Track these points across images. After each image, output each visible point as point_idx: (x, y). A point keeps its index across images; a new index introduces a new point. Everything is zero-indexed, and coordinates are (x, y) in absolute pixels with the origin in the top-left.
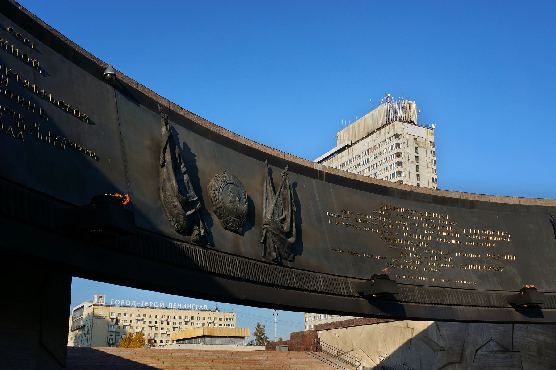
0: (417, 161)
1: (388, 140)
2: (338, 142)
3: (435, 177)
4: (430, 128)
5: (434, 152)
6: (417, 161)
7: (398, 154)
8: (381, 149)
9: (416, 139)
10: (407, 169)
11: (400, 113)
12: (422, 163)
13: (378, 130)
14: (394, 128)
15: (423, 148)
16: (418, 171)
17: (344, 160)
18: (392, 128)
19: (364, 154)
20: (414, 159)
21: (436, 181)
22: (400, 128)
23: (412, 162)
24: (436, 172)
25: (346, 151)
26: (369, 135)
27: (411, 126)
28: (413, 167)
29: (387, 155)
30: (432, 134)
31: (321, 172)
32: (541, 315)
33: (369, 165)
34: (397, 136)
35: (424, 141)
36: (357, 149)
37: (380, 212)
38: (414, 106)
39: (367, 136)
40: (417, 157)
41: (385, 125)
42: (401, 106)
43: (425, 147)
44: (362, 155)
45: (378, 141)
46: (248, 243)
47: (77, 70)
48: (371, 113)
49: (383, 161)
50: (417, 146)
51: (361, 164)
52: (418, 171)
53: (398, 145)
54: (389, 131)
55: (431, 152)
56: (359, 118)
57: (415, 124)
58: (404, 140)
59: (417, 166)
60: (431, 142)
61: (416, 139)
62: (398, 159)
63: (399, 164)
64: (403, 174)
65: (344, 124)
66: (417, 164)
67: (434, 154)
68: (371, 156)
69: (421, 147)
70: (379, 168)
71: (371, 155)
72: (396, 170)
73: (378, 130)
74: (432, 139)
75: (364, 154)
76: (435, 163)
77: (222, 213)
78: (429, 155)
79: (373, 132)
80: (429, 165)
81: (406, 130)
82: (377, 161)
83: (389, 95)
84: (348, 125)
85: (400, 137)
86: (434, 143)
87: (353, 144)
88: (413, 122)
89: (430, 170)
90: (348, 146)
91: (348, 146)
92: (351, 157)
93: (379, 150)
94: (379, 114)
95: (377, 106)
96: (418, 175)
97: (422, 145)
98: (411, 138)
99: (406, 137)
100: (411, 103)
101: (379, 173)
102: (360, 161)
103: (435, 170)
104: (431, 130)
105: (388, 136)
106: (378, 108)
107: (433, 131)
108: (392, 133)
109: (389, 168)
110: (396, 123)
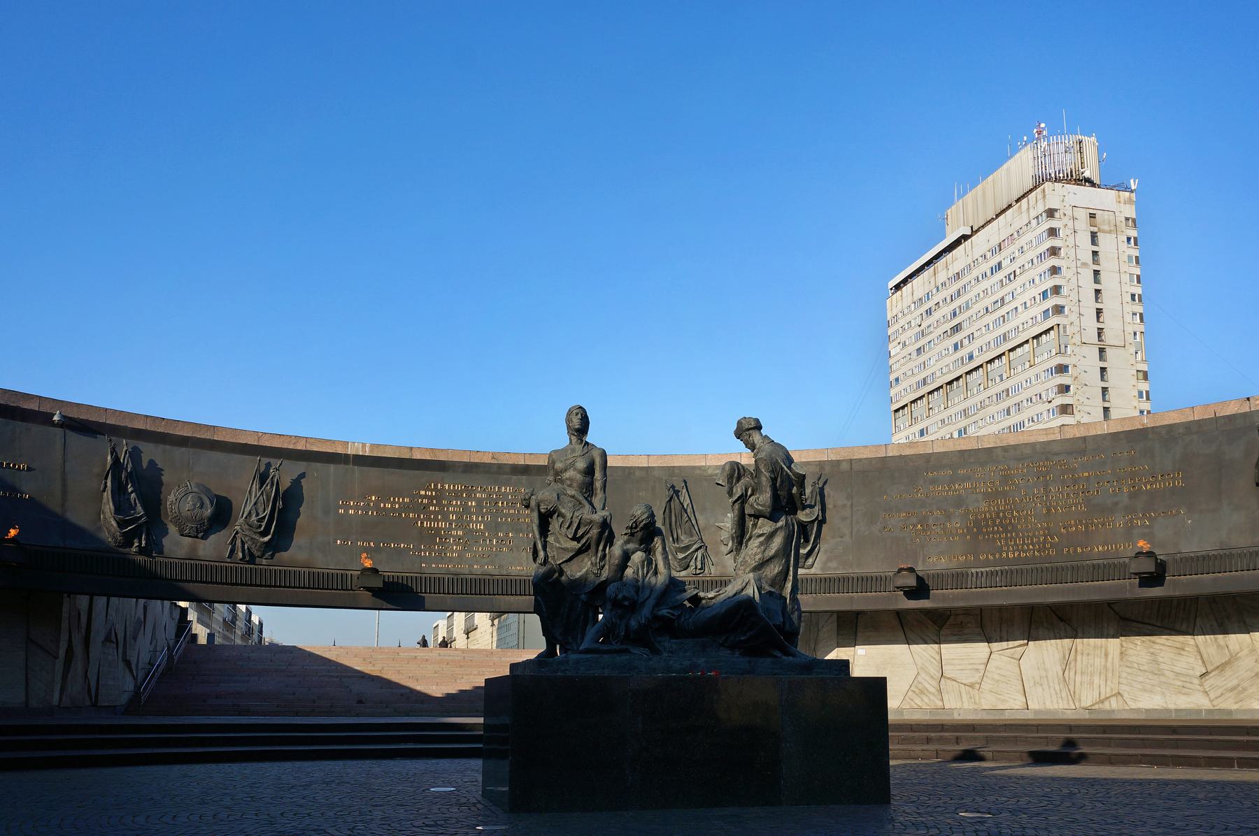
0: (1095, 262)
1: (1034, 222)
2: (948, 229)
3: (1138, 290)
4: (1127, 189)
5: (1135, 239)
6: (1095, 262)
7: (1054, 251)
8: (1023, 241)
9: (1092, 216)
10: (1074, 280)
11: (1067, 163)
12: (1106, 266)
13: (1018, 201)
14: (1044, 197)
15: (1110, 232)
16: (1097, 281)
17: (956, 267)
18: (1040, 196)
19: (993, 251)
20: (1088, 258)
21: (1140, 300)
22: (1056, 195)
23: (1085, 265)
24: (1139, 282)
25: (961, 248)
26: (1003, 211)
27: (1088, 189)
28: (1088, 275)
29: (1032, 254)
30: (1130, 201)
31: (347, 456)
32: (210, 617)
33: (1000, 275)
34: (1051, 213)
35: (1112, 218)
36: (980, 243)
37: (423, 493)
38: (1090, 143)
39: (998, 216)
40: (1095, 253)
41: (1031, 191)
42: (1062, 148)
43: (1116, 230)
44: (989, 254)
45: (1016, 226)
46: (212, 547)
47: (20, 426)
48: (1005, 166)
49: (1027, 267)
50: (1095, 229)
51: (989, 273)
52: (1097, 281)
53: (1053, 232)
54: (1036, 204)
55: (1129, 239)
56: (984, 178)
57: (1093, 184)
58: (1065, 220)
59: (1096, 273)
60: (1127, 219)
61: (1092, 216)
62: (1054, 261)
63: (1055, 270)
64: (1064, 291)
65: (959, 190)
66: (1097, 268)
67: (1136, 244)
68: (1003, 257)
69: (1104, 232)
70: (1020, 280)
71: (1004, 253)
72: (1050, 282)
73: (1018, 201)
74: (1131, 212)
75: (993, 251)
76: (1137, 262)
77: (178, 521)
78: (1123, 246)
79: (1010, 206)
80: (1124, 268)
81: (1071, 200)
82: (1015, 267)
83: (1043, 125)
84: (965, 193)
85: (1057, 215)
86: (1134, 221)
87: (974, 232)
88: (1089, 181)
89: (1126, 278)
90: (965, 237)
91: (965, 237)
92: (970, 261)
93: (1018, 244)
94: (1020, 167)
95: (1015, 150)
96: (1098, 292)
97: (1106, 228)
98: (1083, 216)
99: (1069, 212)
100: (1085, 139)
101: (1019, 290)
102: (985, 267)
103: (1138, 277)
104: (1127, 194)
105: (1033, 214)
106: (1017, 156)
107: (1133, 195)
108: (1041, 208)
109: (1037, 280)
110: (1047, 185)
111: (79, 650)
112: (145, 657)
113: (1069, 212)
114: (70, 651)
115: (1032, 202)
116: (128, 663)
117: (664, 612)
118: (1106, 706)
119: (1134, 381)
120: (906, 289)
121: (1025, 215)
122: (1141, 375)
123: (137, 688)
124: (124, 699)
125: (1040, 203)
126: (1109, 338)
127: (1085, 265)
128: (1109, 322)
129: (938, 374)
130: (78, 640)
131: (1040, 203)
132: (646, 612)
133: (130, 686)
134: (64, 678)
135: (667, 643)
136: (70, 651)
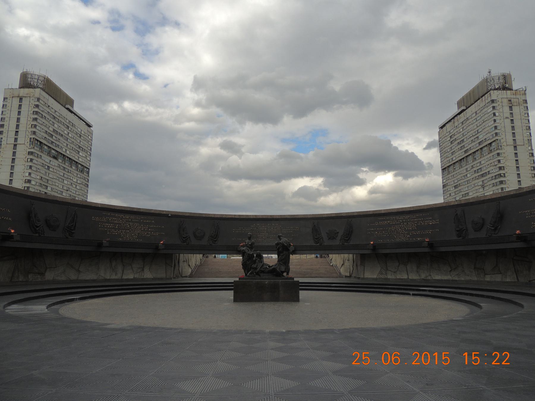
13: (482, 97)
20: (508, 115)
23: (507, 118)
28: (508, 121)
34: (493, 101)
39: (475, 102)
54: (487, 98)
61: (510, 101)
64: (498, 128)
79: (479, 99)
87: (467, 108)
92: (465, 118)
97: (515, 104)
98: (505, 101)
99: (500, 100)
105: (487, 101)
108: (489, 100)
110: (492, 92)
111: (177, 264)
112: (194, 265)
113: (500, 100)
114: (175, 265)
115: (486, 98)
116: (189, 265)
117: (262, 269)
118: (428, 278)
119: (528, 157)
120: (444, 128)
121: (484, 102)
122: (531, 155)
123: (192, 272)
124: (189, 274)
125: (489, 98)
126: (518, 143)
127: (507, 118)
128: (517, 137)
129: (451, 160)
130: (177, 262)
131: (489, 98)
132: (258, 270)
133: (190, 271)
134: (174, 271)
135: (262, 274)
136: (175, 265)
